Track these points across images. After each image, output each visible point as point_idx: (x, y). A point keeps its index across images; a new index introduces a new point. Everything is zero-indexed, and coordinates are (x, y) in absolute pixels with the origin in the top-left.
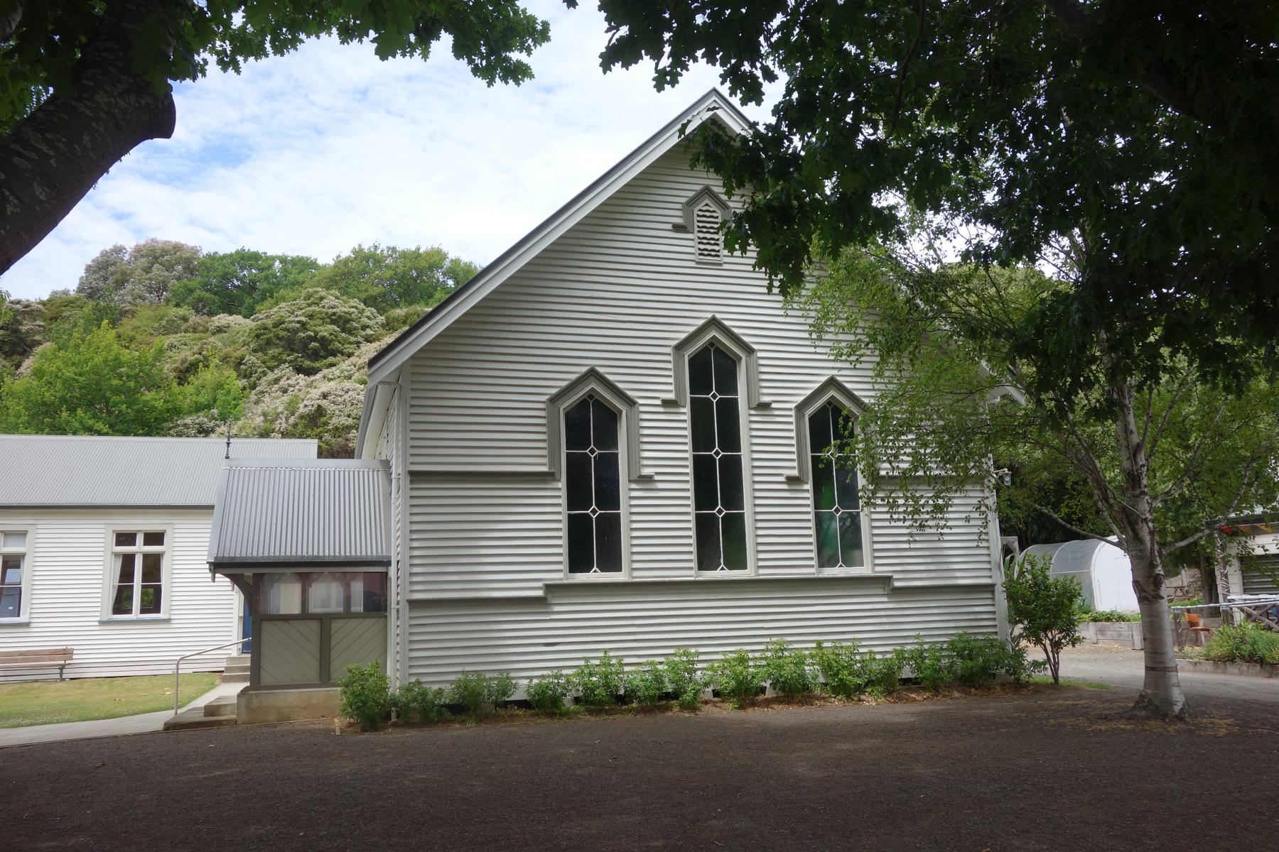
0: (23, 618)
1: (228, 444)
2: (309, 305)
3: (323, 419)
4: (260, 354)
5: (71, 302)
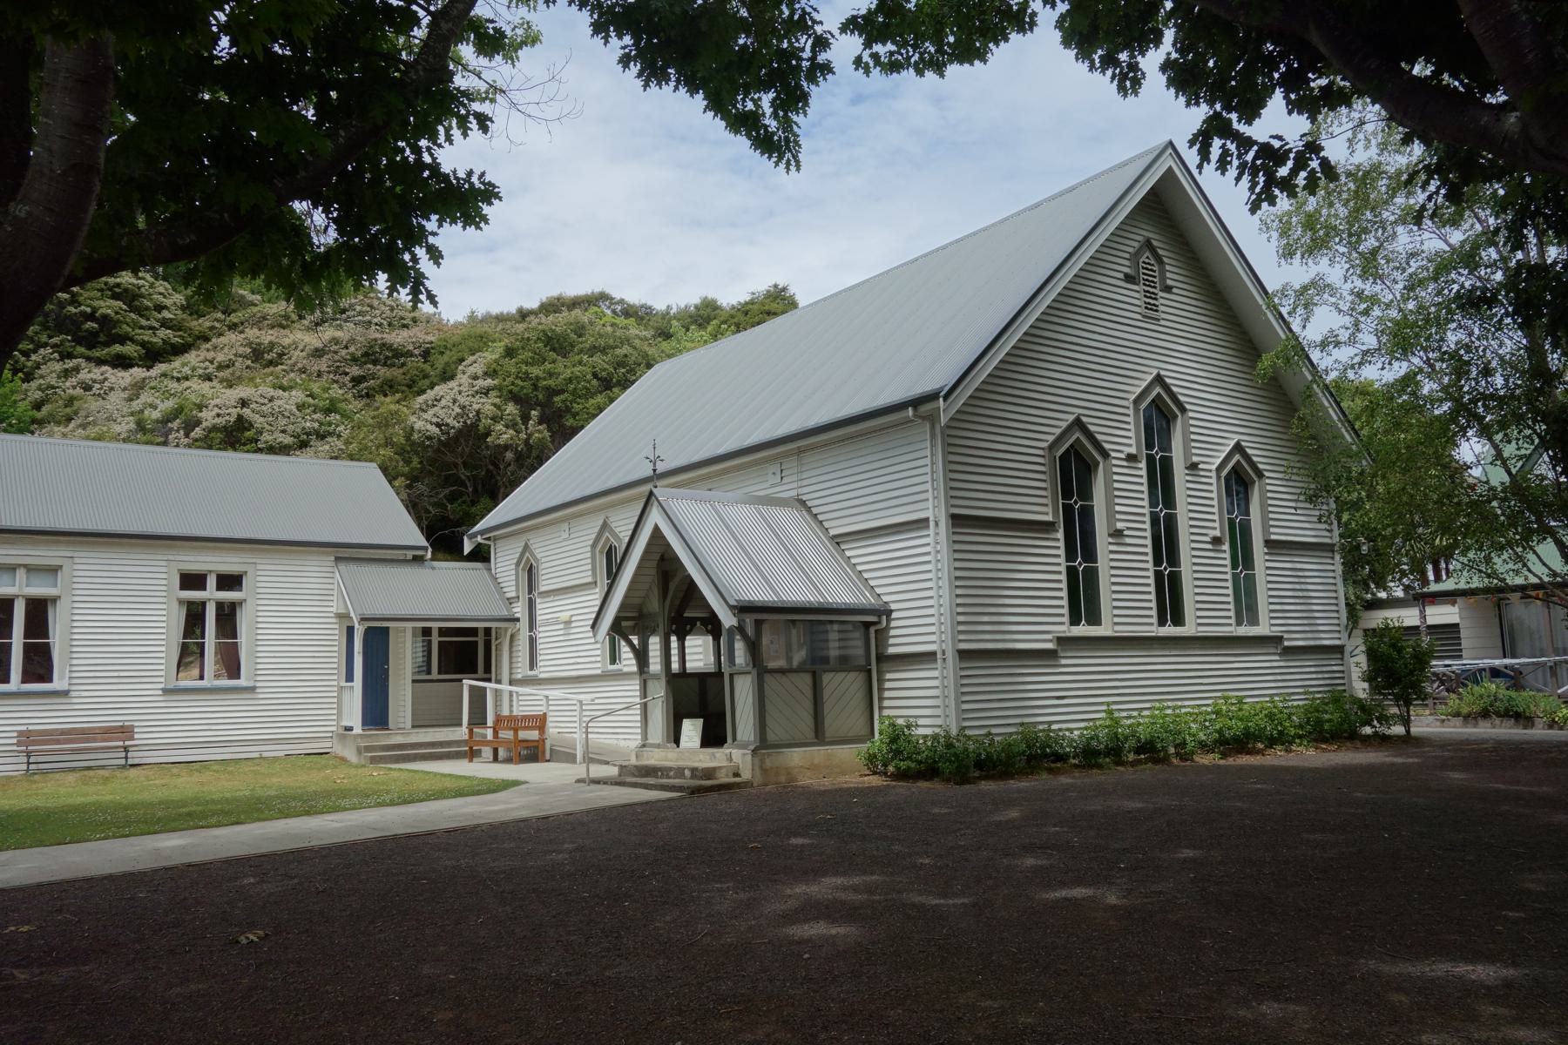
0: (58, 684)
3: (248, 434)
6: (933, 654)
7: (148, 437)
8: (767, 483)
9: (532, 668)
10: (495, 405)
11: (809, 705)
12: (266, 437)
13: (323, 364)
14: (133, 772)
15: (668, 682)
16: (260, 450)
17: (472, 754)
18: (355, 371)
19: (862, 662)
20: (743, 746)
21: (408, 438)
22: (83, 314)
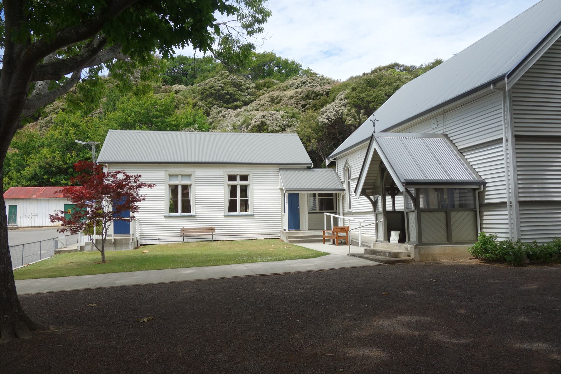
0: (192, 213)
1: (374, 125)
2: (223, 79)
3: (265, 127)
4: (203, 101)
5: (107, 81)
6: (505, 203)
7: (237, 130)
8: (431, 128)
9: (350, 209)
10: (348, 110)
11: (444, 226)
12: (270, 128)
13: (293, 101)
14: (214, 243)
15: (385, 215)
16: (269, 132)
17: (324, 241)
18: (303, 102)
19: (473, 207)
20: (411, 244)
21: (317, 125)
22: (225, 93)
